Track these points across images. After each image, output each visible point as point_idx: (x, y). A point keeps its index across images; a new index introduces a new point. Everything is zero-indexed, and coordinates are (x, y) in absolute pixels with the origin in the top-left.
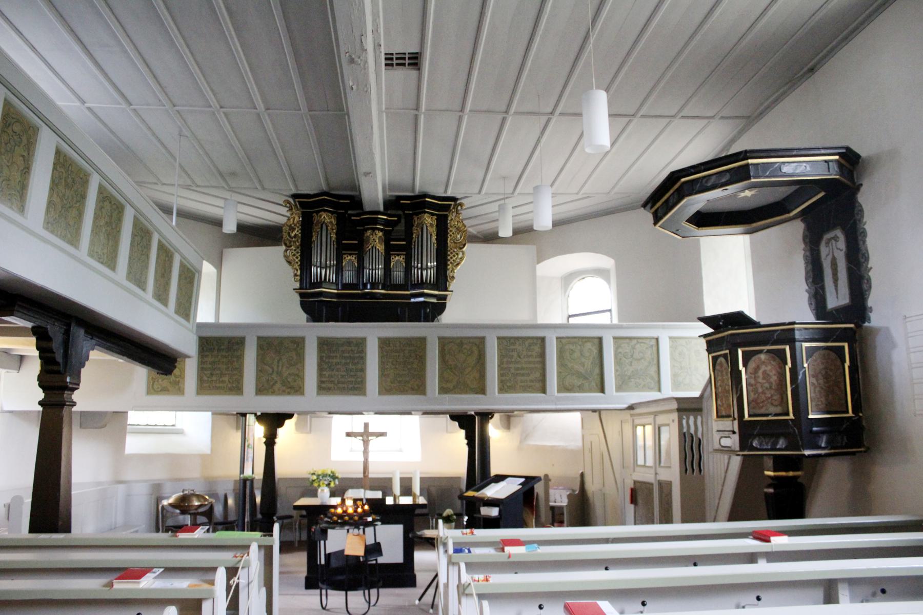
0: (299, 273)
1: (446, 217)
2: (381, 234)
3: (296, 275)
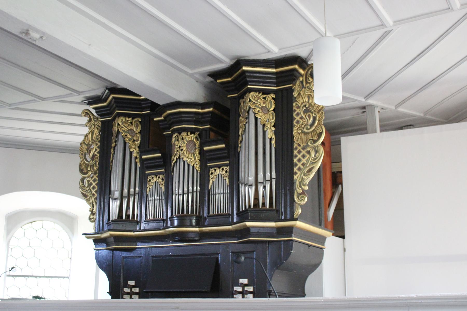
0: (96, 209)
1: (291, 90)
2: (192, 137)
3: (93, 213)
